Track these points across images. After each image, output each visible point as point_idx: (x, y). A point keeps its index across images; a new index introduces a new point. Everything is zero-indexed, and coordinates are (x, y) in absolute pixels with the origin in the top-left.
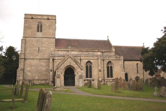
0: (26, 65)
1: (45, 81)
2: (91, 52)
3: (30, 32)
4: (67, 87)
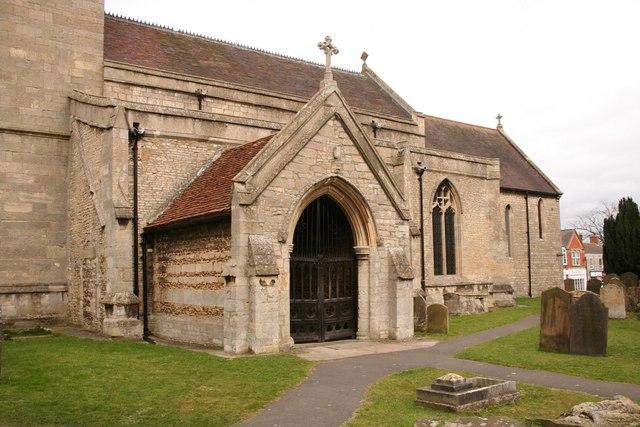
1: (26, 301)
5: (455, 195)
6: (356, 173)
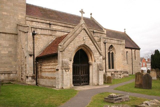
1: (6, 75)
5: (114, 49)
6: (89, 43)
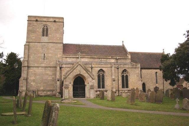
0: (30, 73)
1: (51, 92)
2: (104, 59)
3: (34, 36)
4: (76, 99)
